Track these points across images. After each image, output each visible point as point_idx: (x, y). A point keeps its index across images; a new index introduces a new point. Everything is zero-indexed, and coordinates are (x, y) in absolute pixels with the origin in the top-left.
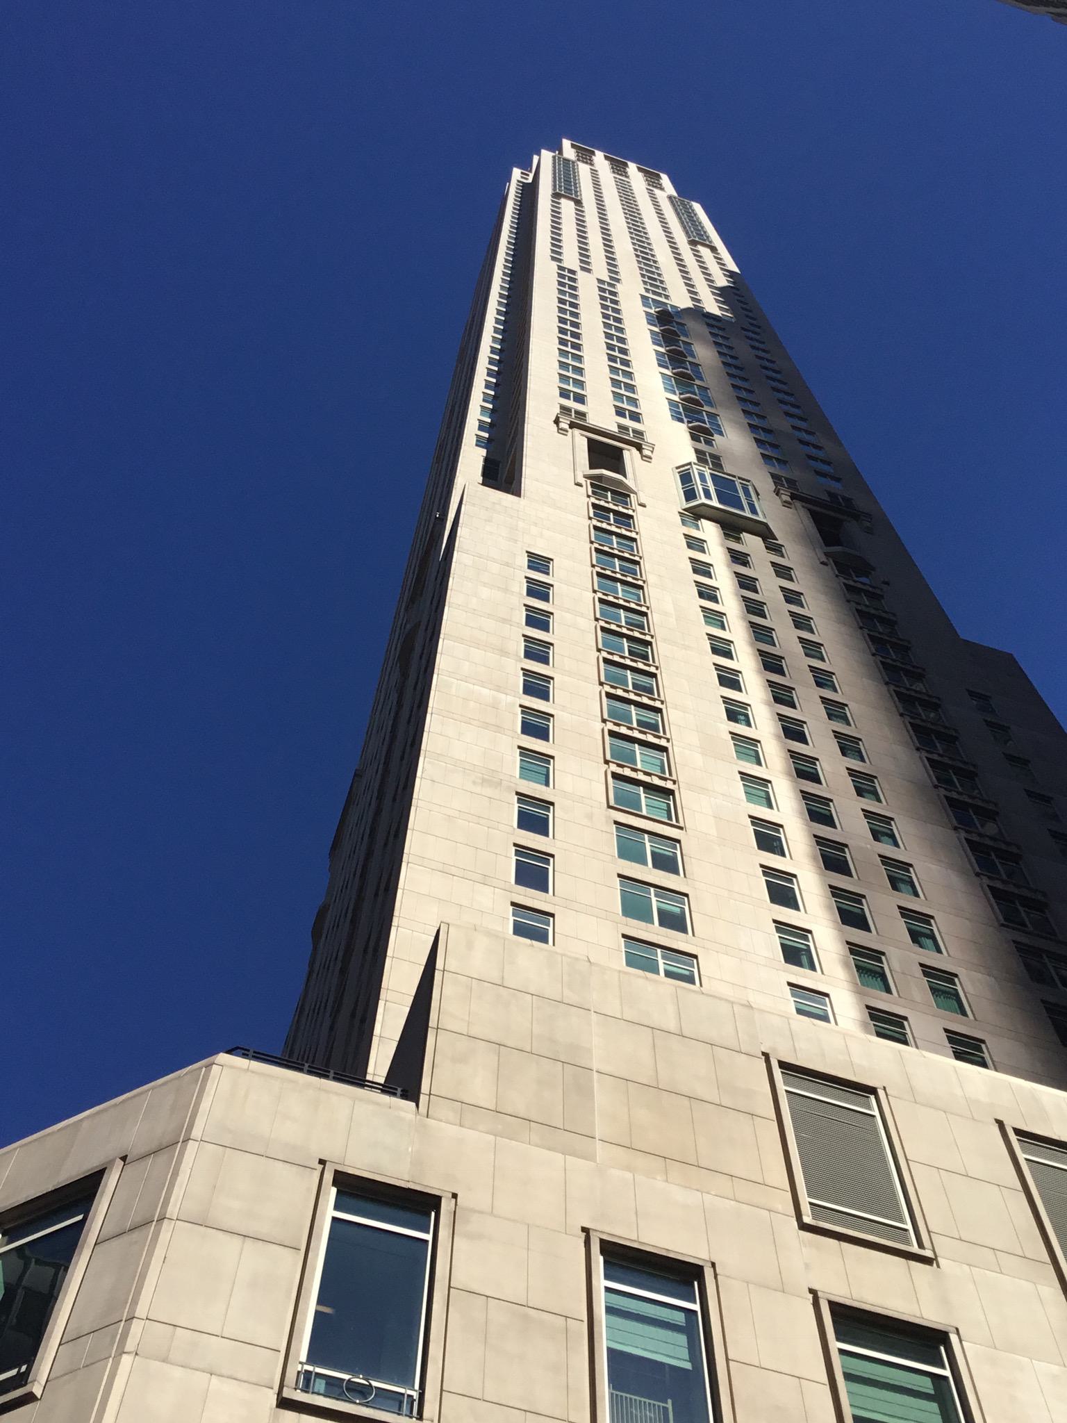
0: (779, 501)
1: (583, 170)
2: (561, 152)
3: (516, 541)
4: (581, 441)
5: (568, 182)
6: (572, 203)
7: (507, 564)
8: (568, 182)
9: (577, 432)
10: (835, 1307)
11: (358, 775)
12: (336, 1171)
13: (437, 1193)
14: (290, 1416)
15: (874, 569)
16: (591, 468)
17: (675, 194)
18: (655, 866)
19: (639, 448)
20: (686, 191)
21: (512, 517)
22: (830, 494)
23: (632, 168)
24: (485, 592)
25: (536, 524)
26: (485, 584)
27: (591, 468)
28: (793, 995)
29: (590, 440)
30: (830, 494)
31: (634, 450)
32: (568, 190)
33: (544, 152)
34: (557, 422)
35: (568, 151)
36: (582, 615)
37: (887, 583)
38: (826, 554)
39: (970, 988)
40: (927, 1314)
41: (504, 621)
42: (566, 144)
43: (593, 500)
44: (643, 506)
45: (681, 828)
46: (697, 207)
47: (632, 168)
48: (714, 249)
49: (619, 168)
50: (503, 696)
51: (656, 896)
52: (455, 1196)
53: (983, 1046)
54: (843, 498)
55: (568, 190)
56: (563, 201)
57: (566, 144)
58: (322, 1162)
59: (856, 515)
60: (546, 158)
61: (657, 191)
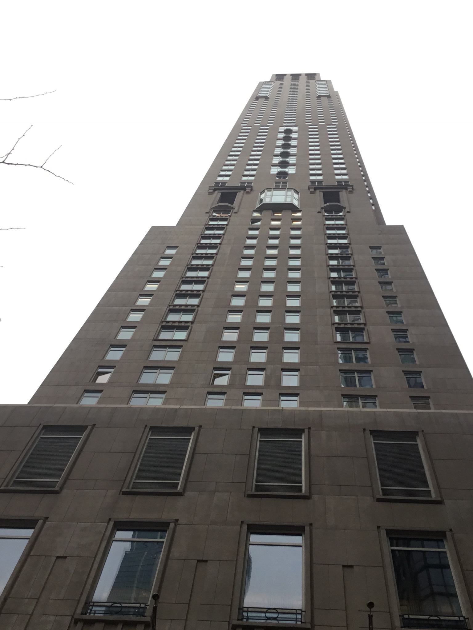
19: (346, 189)
30: (338, 182)
31: (344, 191)
34: (309, 189)
44: (318, 212)
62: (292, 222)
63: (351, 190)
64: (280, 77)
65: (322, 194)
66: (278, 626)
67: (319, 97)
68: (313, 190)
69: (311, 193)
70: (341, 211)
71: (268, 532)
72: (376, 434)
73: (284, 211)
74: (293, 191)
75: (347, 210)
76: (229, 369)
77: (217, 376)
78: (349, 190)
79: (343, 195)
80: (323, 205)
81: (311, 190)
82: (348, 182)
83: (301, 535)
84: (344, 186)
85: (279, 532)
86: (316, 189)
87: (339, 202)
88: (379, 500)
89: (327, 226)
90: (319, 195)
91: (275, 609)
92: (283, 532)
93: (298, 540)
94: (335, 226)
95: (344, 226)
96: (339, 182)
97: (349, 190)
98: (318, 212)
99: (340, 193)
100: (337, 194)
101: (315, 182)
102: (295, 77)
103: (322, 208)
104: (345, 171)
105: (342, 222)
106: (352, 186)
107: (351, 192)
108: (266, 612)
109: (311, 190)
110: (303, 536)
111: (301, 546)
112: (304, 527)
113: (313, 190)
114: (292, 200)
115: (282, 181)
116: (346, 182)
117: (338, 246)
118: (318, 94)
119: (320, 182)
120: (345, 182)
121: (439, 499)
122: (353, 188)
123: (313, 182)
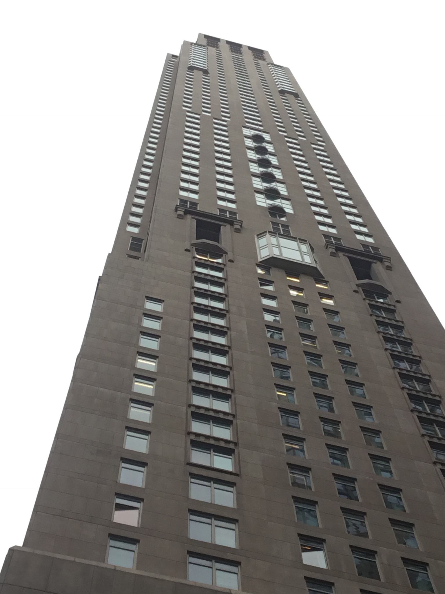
19: (231, 223)
22: (221, 210)
30: (221, 210)
31: (228, 226)
34: (176, 210)
44: (187, 250)
54: (373, 248)
61: (260, 62)
62: (321, 298)
63: (239, 227)
64: (212, 42)
65: (195, 222)
67: (191, 68)
68: (182, 213)
69: (179, 217)
70: (220, 257)
73: (301, 275)
74: (268, 235)
75: (230, 256)
76: (139, 500)
77: (120, 507)
78: (236, 226)
79: (226, 231)
80: (195, 241)
81: (179, 212)
82: (235, 214)
84: (229, 219)
86: (186, 212)
87: (217, 240)
89: (196, 274)
90: (190, 223)
94: (209, 278)
95: (223, 281)
96: (223, 210)
97: (236, 226)
98: (187, 250)
100: (218, 229)
101: (225, 211)
102: (235, 47)
103: (192, 245)
104: (196, 187)
106: (241, 222)
107: (238, 231)
109: (179, 212)
113: (182, 213)
114: (271, 251)
115: (278, 222)
116: (233, 213)
118: (191, 64)
119: (194, 204)
120: (230, 213)
122: (241, 226)
123: (184, 201)
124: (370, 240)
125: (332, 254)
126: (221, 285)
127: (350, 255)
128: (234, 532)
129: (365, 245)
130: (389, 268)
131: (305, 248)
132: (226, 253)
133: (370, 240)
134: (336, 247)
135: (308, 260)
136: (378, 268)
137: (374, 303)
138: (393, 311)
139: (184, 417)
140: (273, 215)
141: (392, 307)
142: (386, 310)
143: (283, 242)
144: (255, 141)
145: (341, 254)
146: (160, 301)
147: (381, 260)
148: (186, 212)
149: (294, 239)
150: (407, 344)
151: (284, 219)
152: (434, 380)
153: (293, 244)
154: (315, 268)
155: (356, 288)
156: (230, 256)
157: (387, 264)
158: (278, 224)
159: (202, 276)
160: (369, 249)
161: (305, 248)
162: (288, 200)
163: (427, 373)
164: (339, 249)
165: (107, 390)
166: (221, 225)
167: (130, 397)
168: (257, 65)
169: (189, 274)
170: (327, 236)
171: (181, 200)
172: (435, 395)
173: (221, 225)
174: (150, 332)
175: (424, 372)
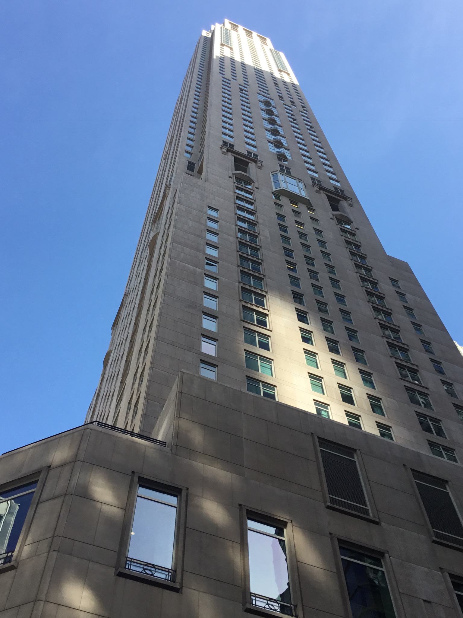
0: (221, 152)
1: (233, 33)
2: (224, 25)
3: (204, 201)
4: (230, 157)
5: (227, 39)
6: (229, 49)
7: (200, 211)
8: (227, 39)
9: (229, 154)
10: (340, 540)
11: (126, 295)
12: (139, 477)
13: (180, 487)
14: (122, 580)
15: (254, 182)
16: (236, 170)
17: (272, 48)
18: (260, 347)
19: (256, 162)
20: (278, 46)
21: (202, 190)
22: (248, 152)
23: (255, 34)
24: (190, 223)
25: (212, 194)
26: (190, 219)
27: (236, 170)
28: (315, 404)
29: (235, 158)
30: (248, 152)
31: (254, 164)
32: (227, 42)
33: (217, 24)
34: (221, 148)
35: (228, 26)
36: (231, 236)
37: (357, 229)
38: (333, 214)
39: (357, 394)
40: (376, 544)
41: (198, 236)
42: (227, 21)
43: (236, 184)
44: (230, 177)
45: (271, 331)
46: (282, 55)
47: (255, 34)
48: (288, 74)
49: (249, 34)
50: (198, 269)
51: (260, 359)
52: (188, 489)
53: (329, 407)
54: (340, 190)
55: (227, 42)
56: (225, 47)
57: (227, 21)
58: (133, 472)
59: (346, 198)
60: (217, 27)
61: (265, 46)
63: (260, 165)
65: (233, 158)
66: (264, 611)
68: (226, 151)
70: (250, 184)
71: (148, 485)
72: (323, 441)
79: (252, 166)
81: (224, 150)
83: (176, 496)
85: (261, 520)
88: (328, 507)
89: (237, 194)
91: (153, 565)
92: (255, 518)
93: (173, 500)
98: (230, 177)
99: (341, 202)
101: (251, 153)
105: (251, 197)
107: (260, 168)
108: (146, 565)
110: (179, 497)
111: (138, 496)
112: (182, 490)
117: (247, 221)
121: (377, 520)
124: (338, 184)
125: (317, 191)
126: (252, 204)
127: (327, 193)
128: (175, 509)
129: (336, 188)
130: (351, 205)
131: (301, 185)
132: (254, 182)
133: (338, 184)
134: (318, 185)
135: (303, 194)
136: (344, 204)
137: (342, 228)
138: (354, 235)
139: (237, 289)
140: (279, 159)
141: (353, 232)
142: (351, 234)
143: (289, 179)
144: (265, 105)
145: (322, 192)
146: (216, 210)
147: (346, 198)
148: (228, 150)
149: (294, 178)
150: (363, 258)
151: (286, 163)
152: (373, 270)
153: (294, 182)
154: (309, 200)
155: (332, 216)
156: (256, 184)
157: (350, 202)
158: (283, 166)
159: (241, 196)
160: (440, 449)
161: (301, 185)
162: (288, 150)
163: (397, 325)
164: (321, 188)
165: (190, 266)
166: (249, 163)
167: (204, 272)
168: (263, 49)
169: (232, 194)
170: (313, 179)
171: (224, 142)
172: (404, 344)
173: (249, 163)
174: (213, 230)
175: (403, 342)
